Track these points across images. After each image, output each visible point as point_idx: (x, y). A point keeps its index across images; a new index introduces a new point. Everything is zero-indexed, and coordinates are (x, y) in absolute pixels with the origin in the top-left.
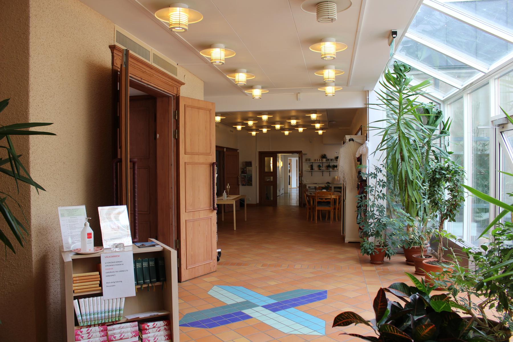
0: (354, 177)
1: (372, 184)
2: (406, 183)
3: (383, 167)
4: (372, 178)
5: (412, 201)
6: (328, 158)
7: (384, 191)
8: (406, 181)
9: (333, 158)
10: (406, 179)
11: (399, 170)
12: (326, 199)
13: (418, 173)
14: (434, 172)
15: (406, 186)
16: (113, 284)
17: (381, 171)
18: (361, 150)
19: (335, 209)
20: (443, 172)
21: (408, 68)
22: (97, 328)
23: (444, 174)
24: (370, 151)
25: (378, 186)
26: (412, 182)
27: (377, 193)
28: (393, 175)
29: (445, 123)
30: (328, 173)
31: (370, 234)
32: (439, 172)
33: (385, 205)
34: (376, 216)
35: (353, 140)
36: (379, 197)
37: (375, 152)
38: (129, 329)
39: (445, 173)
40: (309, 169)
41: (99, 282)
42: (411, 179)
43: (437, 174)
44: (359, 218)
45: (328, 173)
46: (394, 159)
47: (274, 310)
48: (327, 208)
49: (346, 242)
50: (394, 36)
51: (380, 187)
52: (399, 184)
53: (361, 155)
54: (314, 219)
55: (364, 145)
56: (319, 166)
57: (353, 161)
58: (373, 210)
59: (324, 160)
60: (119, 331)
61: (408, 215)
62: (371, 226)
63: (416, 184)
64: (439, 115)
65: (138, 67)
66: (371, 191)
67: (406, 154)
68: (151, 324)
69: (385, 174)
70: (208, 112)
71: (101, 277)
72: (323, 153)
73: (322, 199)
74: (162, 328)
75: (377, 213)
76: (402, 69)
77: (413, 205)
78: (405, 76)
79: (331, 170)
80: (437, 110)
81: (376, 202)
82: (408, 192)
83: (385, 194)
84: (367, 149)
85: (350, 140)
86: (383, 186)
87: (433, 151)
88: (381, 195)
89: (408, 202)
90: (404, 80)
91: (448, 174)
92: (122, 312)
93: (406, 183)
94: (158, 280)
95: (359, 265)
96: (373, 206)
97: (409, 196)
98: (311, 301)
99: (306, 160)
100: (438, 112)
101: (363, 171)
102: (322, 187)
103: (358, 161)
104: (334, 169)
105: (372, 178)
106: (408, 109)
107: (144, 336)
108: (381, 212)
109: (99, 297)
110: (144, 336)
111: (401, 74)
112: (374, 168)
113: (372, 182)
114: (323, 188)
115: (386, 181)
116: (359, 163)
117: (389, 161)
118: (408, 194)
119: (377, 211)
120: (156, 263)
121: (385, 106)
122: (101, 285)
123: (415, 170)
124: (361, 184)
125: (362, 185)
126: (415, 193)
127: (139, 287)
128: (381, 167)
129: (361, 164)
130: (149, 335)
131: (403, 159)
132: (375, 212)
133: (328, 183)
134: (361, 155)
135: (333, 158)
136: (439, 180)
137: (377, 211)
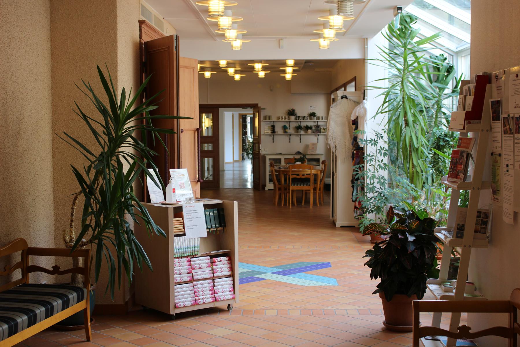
0: (347, 144)
1: (372, 152)
2: (410, 151)
3: (385, 132)
4: (372, 145)
5: (417, 172)
6: (298, 115)
7: (386, 160)
8: (410, 148)
9: (306, 115)
10: (410, 146)
11: (404, 135)
12: (303, 175)
13: (424, 140)
14: (439, 138)
15: (410, 155)
16: (192, 227)
17: (382, 137)
18: (357, 111)
19: (315, 189)
20: (447, 139)
21: (412, 18)
22: (184, 260)
23: (448, 141)
24: (370, 113)
25: (379, 155)
26: (417, 149)
27: (377, 163)
28: (395, 141)
29: (458, 79)
30: (298, 138)
31: (369, 210)
32: (443, 139)
33: (386, 177)
34: (377, 190)
35: (346, 97)
36: (380, 167)
37: (375, 116)
38: (204, 261)
39: (449, 140)
40: (270, 132)
41: (182, 226)
42: (416, 146)
43: (441, 140)
44: (354, 194)
45: (298, 138)
46: (397, 123)
47: (285, 275)
48: (304, 187)
49: (337, 226)
50: (399, 11)
51: (381, 155)
52: (403, 152)
53: (357, 117)
54: (285, 204)
55: (361, 105)
56: (285, 128)
57: (347, 124)
58: (374, 183)
59: (293, 118)
60: (198, 262)
61: (413, 185)
62: (372, 201)
63: (422, 152)
64: (450, 70)
65: (149, 33)
66: (371, 160)
67: (411, 119)
68: (219, 259)
69: (387, 140)
70: (192, 70)
71: (183, 222)
72: (291, 108)
73: (298, 175)
74: (226, 262)
75: (378, 186)
76: (408, 20)
77: (418, 176)
78: (410, 27)
79: (302, 132)
80: (448, 64)
81: (376, 174)
82: (412, 161)
83: (387, 163)
84: (365, 110)
85: (342, 97)
86: (385, 154)
87: (444, 114)
88: (382, 165)
89: (413, 173)
90: (410, 31)
91: (451, 141)
92: (199, 248)
93: (410, 151)
94: (220, 226)
95: (358, 245)
96: (374, 177)
97: (413, 166)
98: (317, 269)
99: (265, 118)
100: (450, 66)
101: (360, 137)
102: (295, 159)
103: (353, 124)
104: (306, 132)
105: (372, 145)
106: (414, 67)
107: (214, 267)
108: (382, 184)
109: (183, 237)
110: (214, 267)
111: (407, 26)
112: (374, 133)
113: (370, 150)
114: (297, 160)
115: (387, 149)
116: (354, 127)
117: (391, 125)
118: (413, 163)
119: (378, 183)
120: (218, 213)
121: (387, 62)
122: (184, 228)
123: (420, 136)
124: (357, 153)
125: (358, 155)
126: (420, 162)
127: (208, 230)
128: (382, 132)
129: (357, 128)
130: (217, 267)
131: (407, 124)
132: (375, 185)
133: (299, 153)
134: (357, 117)
135: (306, 115)
136: (444, 147)
137: (378, 183)
